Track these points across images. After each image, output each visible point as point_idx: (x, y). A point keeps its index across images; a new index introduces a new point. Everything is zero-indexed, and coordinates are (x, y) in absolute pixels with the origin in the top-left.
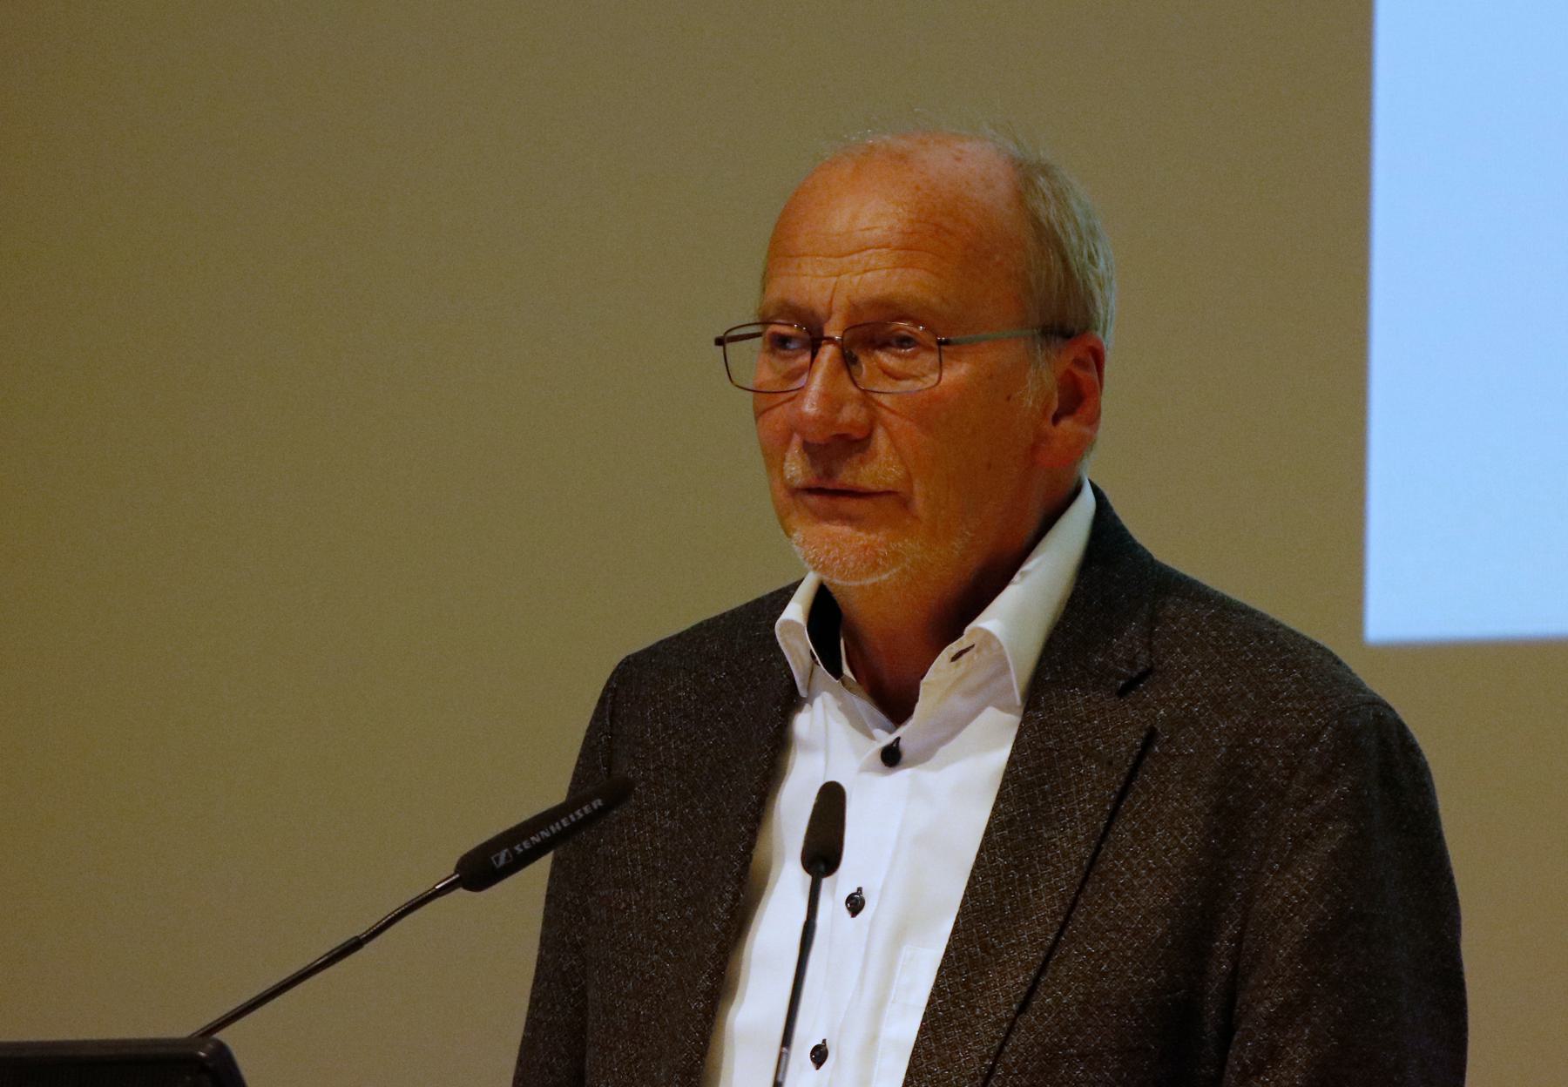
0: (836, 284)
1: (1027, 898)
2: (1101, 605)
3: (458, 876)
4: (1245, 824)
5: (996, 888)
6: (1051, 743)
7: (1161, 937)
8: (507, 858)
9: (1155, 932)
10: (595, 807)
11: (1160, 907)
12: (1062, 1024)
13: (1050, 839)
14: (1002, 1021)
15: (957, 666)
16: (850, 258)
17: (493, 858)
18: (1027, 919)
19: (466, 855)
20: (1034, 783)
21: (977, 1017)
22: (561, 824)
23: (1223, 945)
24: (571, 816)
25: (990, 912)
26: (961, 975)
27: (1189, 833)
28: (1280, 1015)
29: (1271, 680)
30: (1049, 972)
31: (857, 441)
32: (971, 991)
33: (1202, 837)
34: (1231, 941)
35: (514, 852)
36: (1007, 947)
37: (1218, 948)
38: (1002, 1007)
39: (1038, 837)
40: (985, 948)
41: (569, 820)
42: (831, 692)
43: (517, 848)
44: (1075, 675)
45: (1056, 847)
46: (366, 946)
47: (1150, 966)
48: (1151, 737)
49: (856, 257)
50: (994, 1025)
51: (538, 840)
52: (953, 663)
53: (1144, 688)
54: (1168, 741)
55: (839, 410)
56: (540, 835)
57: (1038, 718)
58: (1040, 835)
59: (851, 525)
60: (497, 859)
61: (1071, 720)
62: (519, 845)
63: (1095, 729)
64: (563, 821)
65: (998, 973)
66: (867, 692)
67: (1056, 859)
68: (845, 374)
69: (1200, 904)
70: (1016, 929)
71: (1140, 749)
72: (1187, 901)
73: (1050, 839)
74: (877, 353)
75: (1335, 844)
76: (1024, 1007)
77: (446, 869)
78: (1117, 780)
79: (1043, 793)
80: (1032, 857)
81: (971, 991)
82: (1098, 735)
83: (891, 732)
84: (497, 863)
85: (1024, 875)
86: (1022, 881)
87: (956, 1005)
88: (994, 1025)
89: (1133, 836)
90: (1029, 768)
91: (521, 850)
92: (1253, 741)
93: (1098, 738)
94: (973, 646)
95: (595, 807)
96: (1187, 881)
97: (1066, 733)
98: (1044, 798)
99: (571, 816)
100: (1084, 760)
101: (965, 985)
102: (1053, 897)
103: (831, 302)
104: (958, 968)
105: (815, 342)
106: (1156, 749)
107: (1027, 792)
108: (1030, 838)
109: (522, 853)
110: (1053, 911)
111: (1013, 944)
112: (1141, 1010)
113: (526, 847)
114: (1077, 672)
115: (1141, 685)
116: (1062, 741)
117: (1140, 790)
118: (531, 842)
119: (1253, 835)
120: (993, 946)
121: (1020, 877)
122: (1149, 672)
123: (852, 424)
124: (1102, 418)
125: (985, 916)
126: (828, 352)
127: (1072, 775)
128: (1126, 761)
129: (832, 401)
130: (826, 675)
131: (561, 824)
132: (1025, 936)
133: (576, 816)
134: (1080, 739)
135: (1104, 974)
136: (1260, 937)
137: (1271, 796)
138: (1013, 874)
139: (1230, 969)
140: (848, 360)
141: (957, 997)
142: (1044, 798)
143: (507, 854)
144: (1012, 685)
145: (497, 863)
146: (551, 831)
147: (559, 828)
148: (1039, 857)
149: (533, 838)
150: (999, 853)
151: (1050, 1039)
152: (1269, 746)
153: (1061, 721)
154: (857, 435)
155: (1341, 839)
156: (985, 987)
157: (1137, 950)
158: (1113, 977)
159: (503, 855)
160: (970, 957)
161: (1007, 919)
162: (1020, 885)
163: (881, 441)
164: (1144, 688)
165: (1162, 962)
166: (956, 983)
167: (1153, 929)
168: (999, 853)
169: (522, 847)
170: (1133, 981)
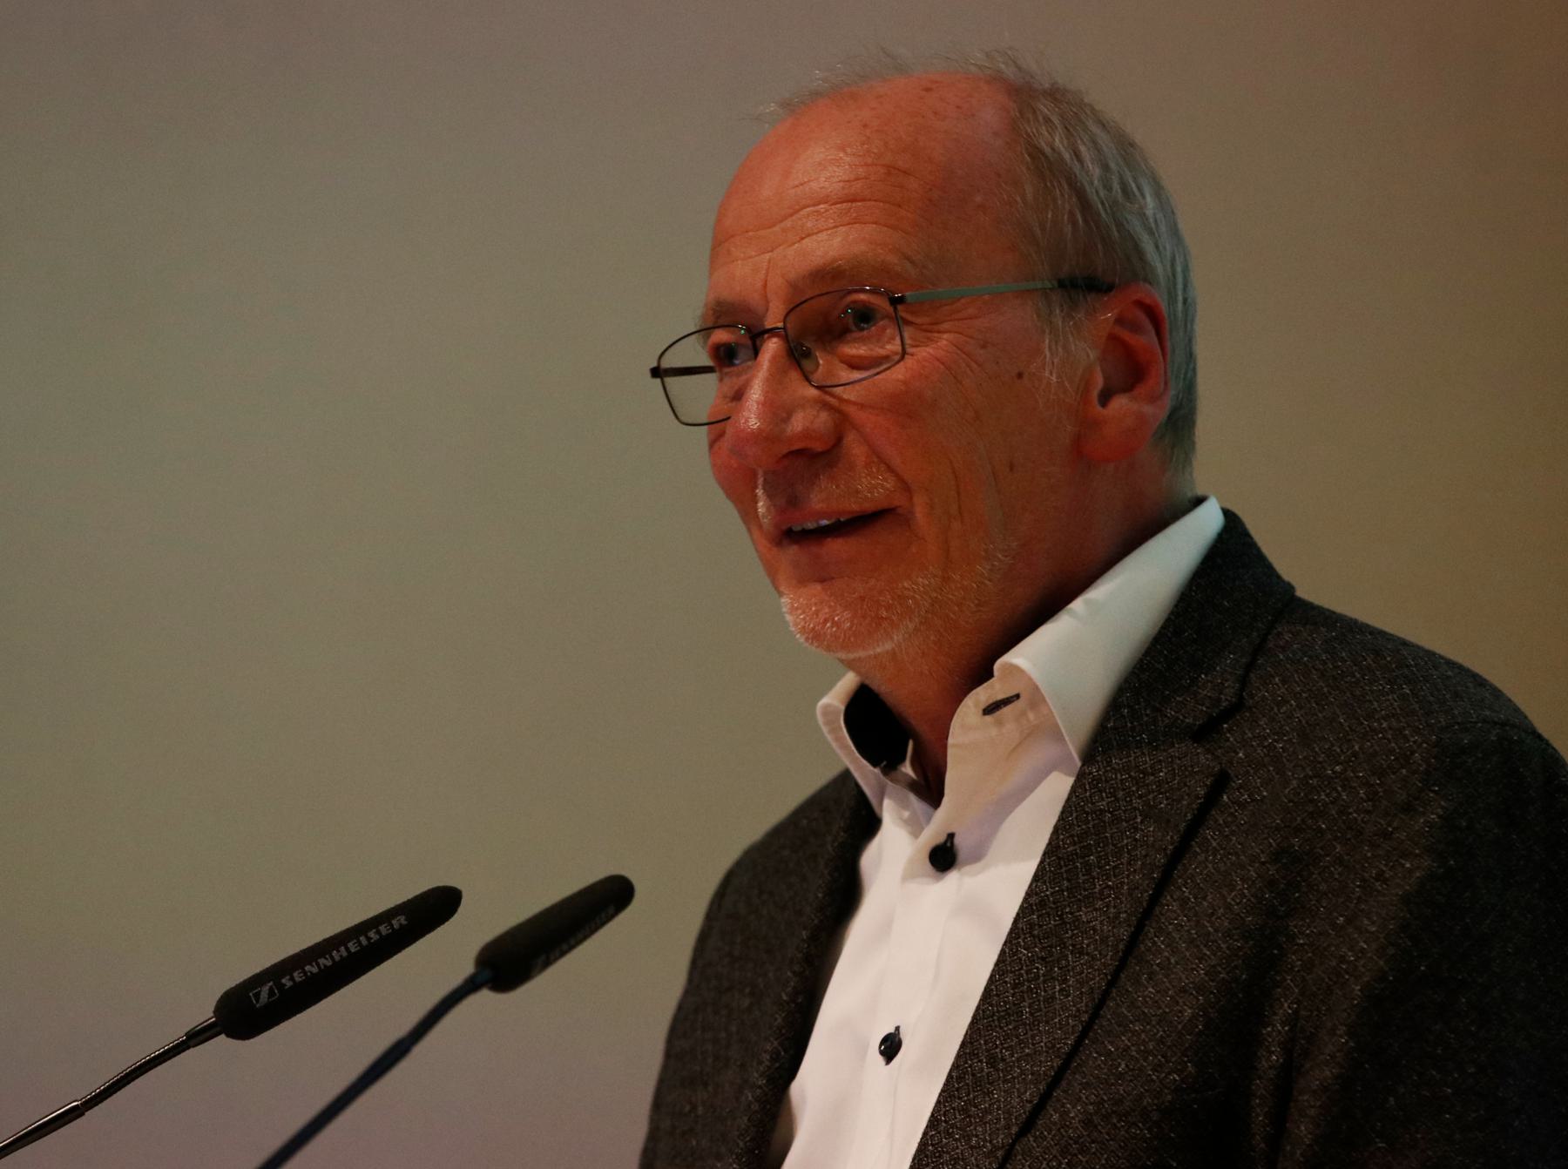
0: (769, 261)
1: (1053, 998)
2: (1195, 636)
3: (214, 1019)
4: (1313, 873)
5: (1015, 986)
6: (1104, 803)
7: (1189, 1020)
9: (1183, 1016)
11: (1192, 983)
12: (1063, 1142)
13: (1088, 922)
14: (998, 1149)
15: (1000, 723)
16: (782, 225)
18: (1047, 1022)
20: (1076, 854)
21: (972, 1147)
22: (347, 949)
23: (1276, 1029)
24: (362, 939)
25: (1003, 1017)
26: (960, 1098)
27: (1238, 888)
28: (1312, 1103)
29: (1371, 698)
30: (1064, 1083)
31: (822, 453)
32: (969, 1116)
33: (1254, 890)
34: (1283, 1024)
35: (281, 987)
36: (1018, 1060)
37: (1269, 1034)
38: (1001, 1132)
39: (1074, 922)
40: (992, 1062)
41: (359, 943)
43: (286, 981)
44: (1145, 719)
45: (1094, 930)
47: (1173, 1060)
48: (1221, 782)
49: (788, 223)
50: (988, 1155)
51: (315, 970)
52: (988, 718)
53: (1229, 730)
54: (1241, 786)
55: (787, 420)
56: (318, 965)
57: (1092, 773)
58: (1078, 919)
60: (257, 996)
61: (1132, 774)
62: (288, 977)
63: (1160, 783)
65: (1004, 1092)
67: (1092, 947)
68: (794, 375)
69: (1244, 976)
70: (1033, 1037)
71: (1202, 800)
72: (1228, 973)
73: (1088, 922)
75: (1410, 885)
76: (1027, 1127)
77: (203, 1012)
78: (1170, 839)
79: (1087, 865)
80: (1063, 945)
81: (969, 1116)
82: (1162, 790)
84: (257, 1001)
85: (1051, 969)
86: (1049, 977)
87: (950, 1135)
88: (988, 1155)
89: (1181, 905)
90: (1072, 836)
92: (1332, 770)
93: (1161, 793)
94: (1018, 696)
96: (1228, 948)
97: (1124, 790)
98: (1088, 872)
99: (362, 939)
100: (1142, 822)
101: (964, 1110)
102: (1082, 993)
103: (765, 286)
104: (957, 1090)
105: (757, 336)
106: (1225, 797)
107: (1066, 866)
108: (1065, 923)
110: (1078, 1010)
111: (1028, 1055)
112: (1155, 1116)
114: (1147, 715)
115: (1225, 726)
116: (1117, 800)
117: (1198, 850)
119: (1323, 887)
120: (1003, 1060)
121: (1047, 971)
122: (1237, 707)
123: (806, 434)
125: (996, 1023)
126: (772, 346)
127: (1125, 841)
128: (1185, 816)
129: (777, 411)
130: (854, 753)
131: (347, 949)
132: (1042, 1044)
133: (369, 939)
134: (1140, 797)
135: (1120, 1076)
136: (1315, 1013)
137: (1349, 836)
138: (1037, 968)
139: (1281, 1060)
140: (797, 356)
141: (952, 1126)
142: (1088, 872)
143: (271, 989)
147: (345, 954)
148: (1073, 946)
149: (307, 968)
150: (1022, 944)
151: (1048, 1164)
152: (1352, 775)
153: (1119, 776)
154: (818, 447)
155: (1418, 878)
156: (987, 1111)
157: (1161, 1041)
158: (1129, 1078)
159: (265, 990)
160: (973, 1075)
161: (1025, 1024)
162: (1044, 982)
163: (854, 448)
164: (1229, 730)
165: (1189, 1053)
166: (954, 1109)
167: (1180, 1012)
168: (1022, 944)
170: (1152, 1080)
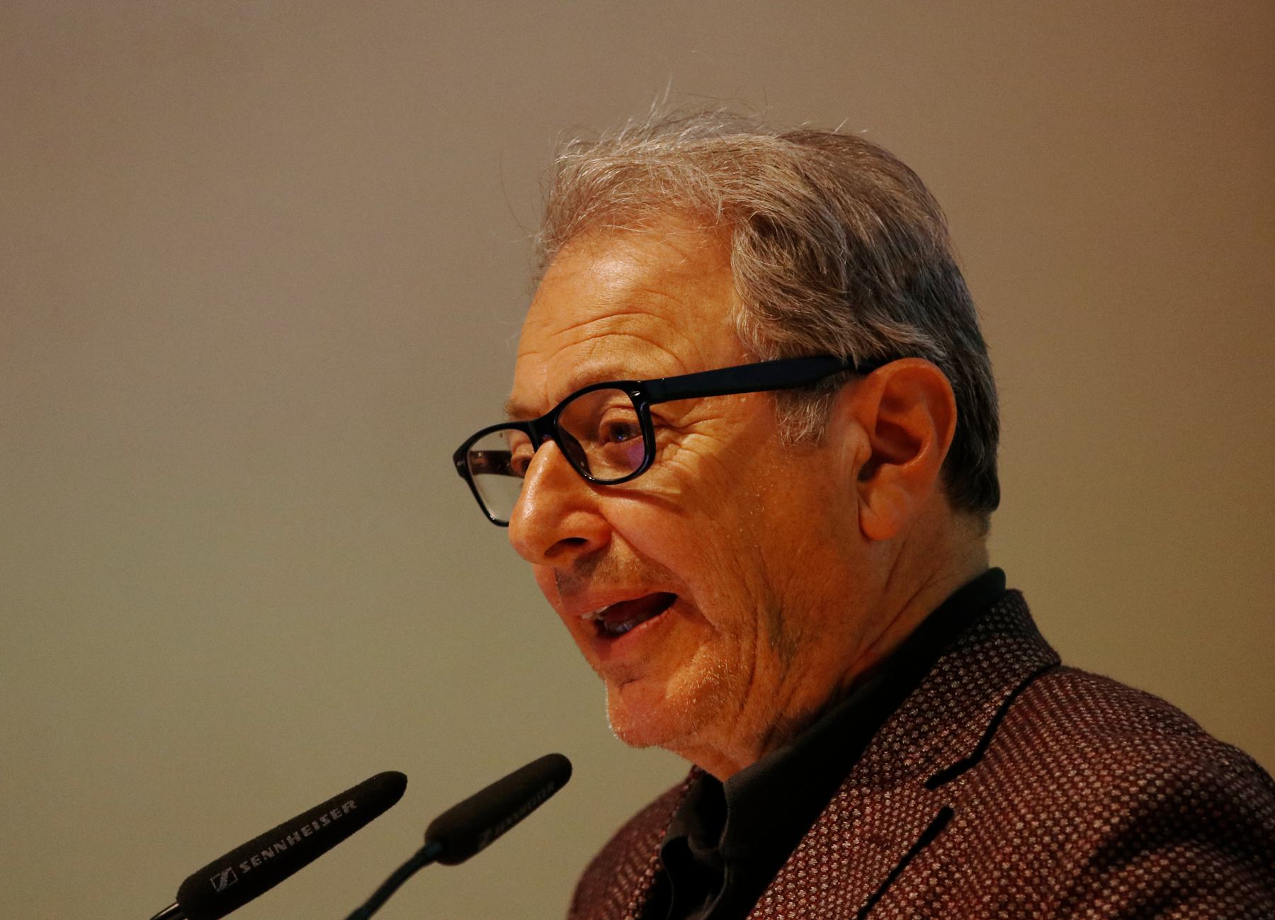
8: (230, 878)
19: (186, 880)
22: (301, 834)
35: (239, 872)
51: (271, 854)
59: (523, 508)
60: (217, 881)
77: (463, 483)
83: (803, 283)
84: (218, 887)
91: (247, 869)
113: (255, 864)
118: (262, 857)
124: (545, 600)
133: (320, 823)
143: (230, 874)
144: (938, 331)
145: (218, 887)
149: (264, 853)
159: (224, 876)
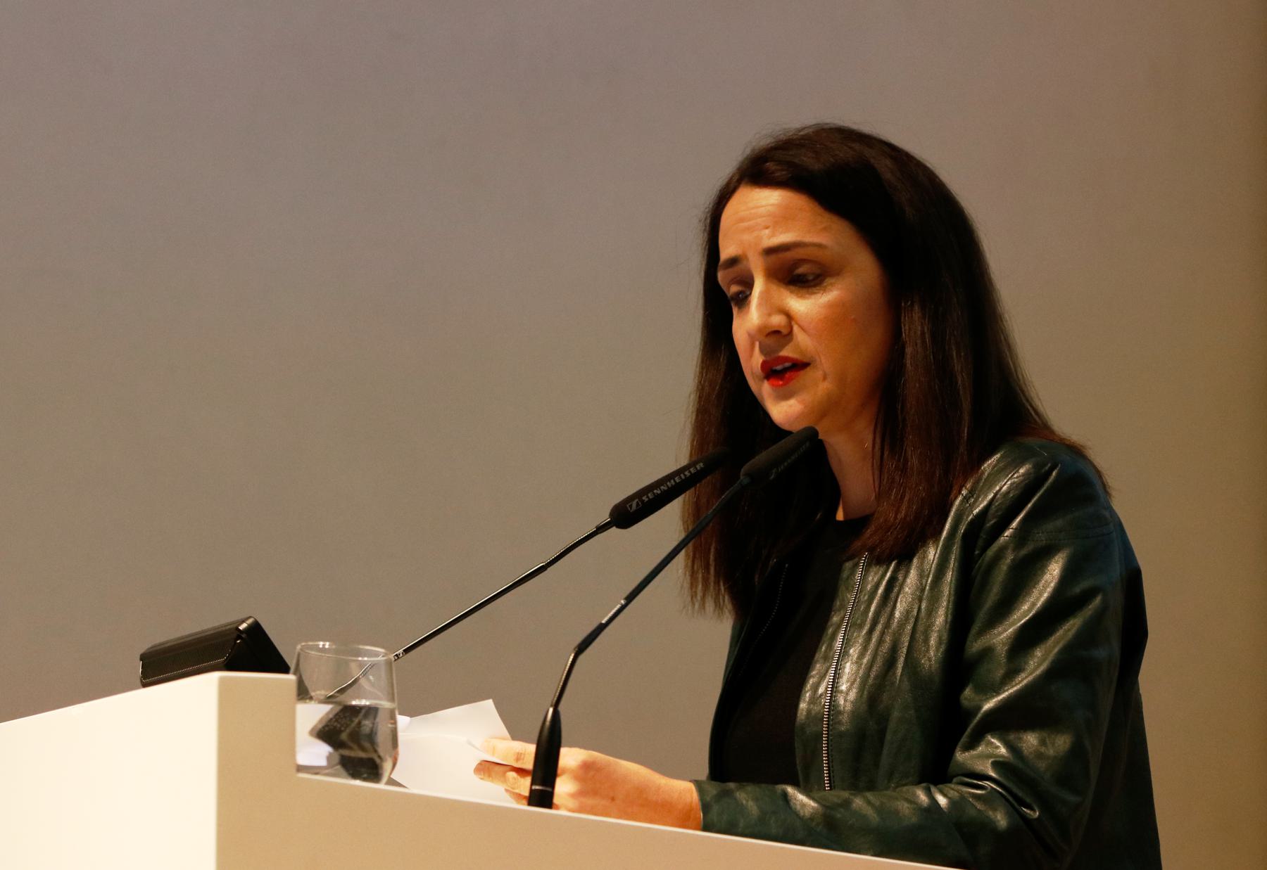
10: (699, 468)
17: (628, 506)
22: (675, 481)
35: (643, 501)
41: (681, 477)
42: (1032, 471)
46: (549, 569)
51: (659, 492)
60: (631, 506)
64: (676, 479)
66: (749, 308)
74: (839, 802)
77: (605, 517)
91: (647, 500)
95: (699, 468)
99: (682, 475)
109: (690, 476)
113: (651, 497)
131: (675, 481)
133: (685, 475)
143: (637, 502)
145: (631, 509)
146: (667, 486)
169: (648, 497)
